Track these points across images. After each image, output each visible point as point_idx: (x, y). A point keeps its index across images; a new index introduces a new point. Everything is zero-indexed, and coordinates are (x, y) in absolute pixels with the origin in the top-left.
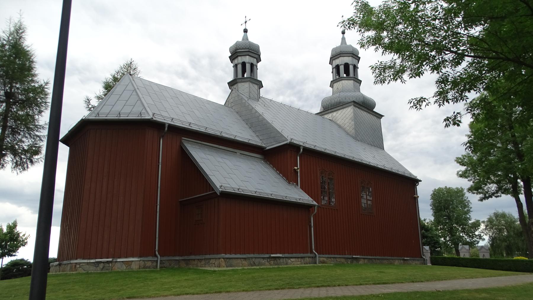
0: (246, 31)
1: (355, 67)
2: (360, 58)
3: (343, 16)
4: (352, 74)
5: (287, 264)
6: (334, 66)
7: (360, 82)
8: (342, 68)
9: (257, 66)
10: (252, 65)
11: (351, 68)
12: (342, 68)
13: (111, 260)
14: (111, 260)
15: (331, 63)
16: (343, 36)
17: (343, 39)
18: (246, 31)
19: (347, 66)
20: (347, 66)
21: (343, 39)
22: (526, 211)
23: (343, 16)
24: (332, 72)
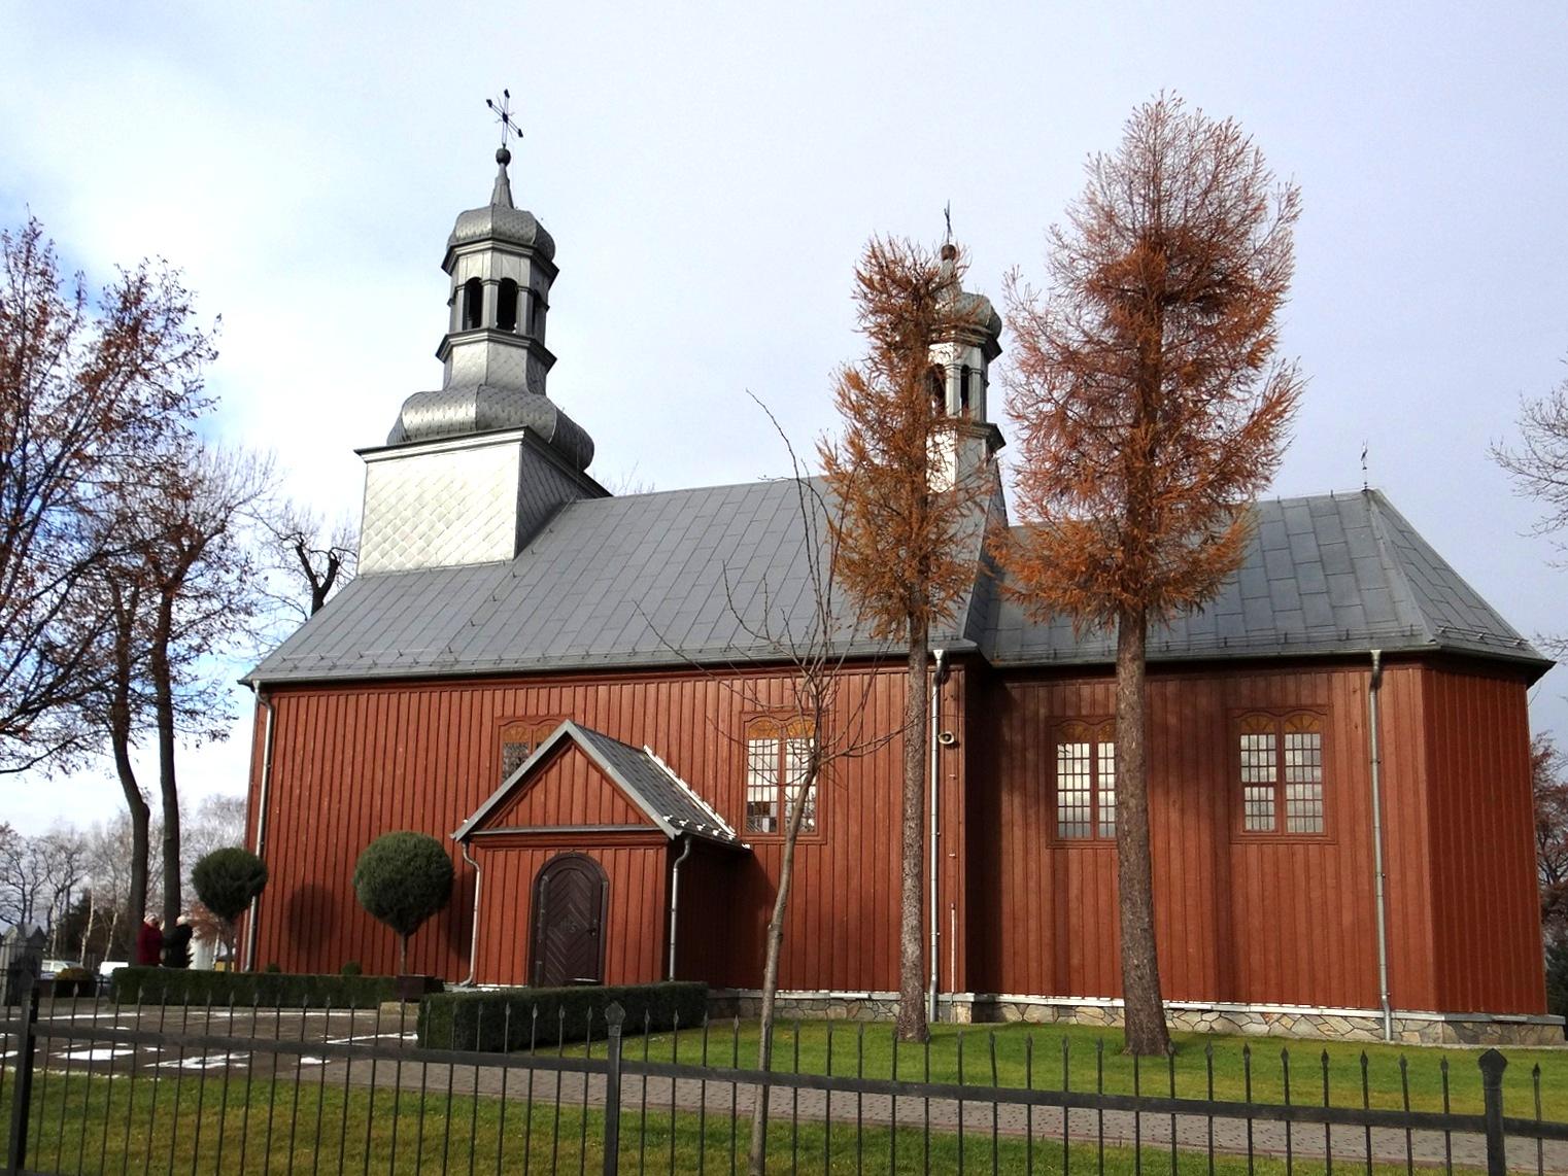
0: (504, 158)
1: (539, 305)
2: (557, 271)
3: (490, 103)
4: (521, 325)
5: (749, 1137)
6: (462, 281)
7: (548, 360)
8: (490, 295)
9: (984, 375)
10: (966, 372)
11: (523, 299)
12: (490, 295)
13: (864, 995)
14: (864, 995)
15: (450, 264)
16: (504, 174)
17: (504, 181)
18: (504, 158)
19: (507, 288)
20: (507, 288)
21: (504, 181)
22: (687, 983)
23: (490, 103)
24: (452, 302)
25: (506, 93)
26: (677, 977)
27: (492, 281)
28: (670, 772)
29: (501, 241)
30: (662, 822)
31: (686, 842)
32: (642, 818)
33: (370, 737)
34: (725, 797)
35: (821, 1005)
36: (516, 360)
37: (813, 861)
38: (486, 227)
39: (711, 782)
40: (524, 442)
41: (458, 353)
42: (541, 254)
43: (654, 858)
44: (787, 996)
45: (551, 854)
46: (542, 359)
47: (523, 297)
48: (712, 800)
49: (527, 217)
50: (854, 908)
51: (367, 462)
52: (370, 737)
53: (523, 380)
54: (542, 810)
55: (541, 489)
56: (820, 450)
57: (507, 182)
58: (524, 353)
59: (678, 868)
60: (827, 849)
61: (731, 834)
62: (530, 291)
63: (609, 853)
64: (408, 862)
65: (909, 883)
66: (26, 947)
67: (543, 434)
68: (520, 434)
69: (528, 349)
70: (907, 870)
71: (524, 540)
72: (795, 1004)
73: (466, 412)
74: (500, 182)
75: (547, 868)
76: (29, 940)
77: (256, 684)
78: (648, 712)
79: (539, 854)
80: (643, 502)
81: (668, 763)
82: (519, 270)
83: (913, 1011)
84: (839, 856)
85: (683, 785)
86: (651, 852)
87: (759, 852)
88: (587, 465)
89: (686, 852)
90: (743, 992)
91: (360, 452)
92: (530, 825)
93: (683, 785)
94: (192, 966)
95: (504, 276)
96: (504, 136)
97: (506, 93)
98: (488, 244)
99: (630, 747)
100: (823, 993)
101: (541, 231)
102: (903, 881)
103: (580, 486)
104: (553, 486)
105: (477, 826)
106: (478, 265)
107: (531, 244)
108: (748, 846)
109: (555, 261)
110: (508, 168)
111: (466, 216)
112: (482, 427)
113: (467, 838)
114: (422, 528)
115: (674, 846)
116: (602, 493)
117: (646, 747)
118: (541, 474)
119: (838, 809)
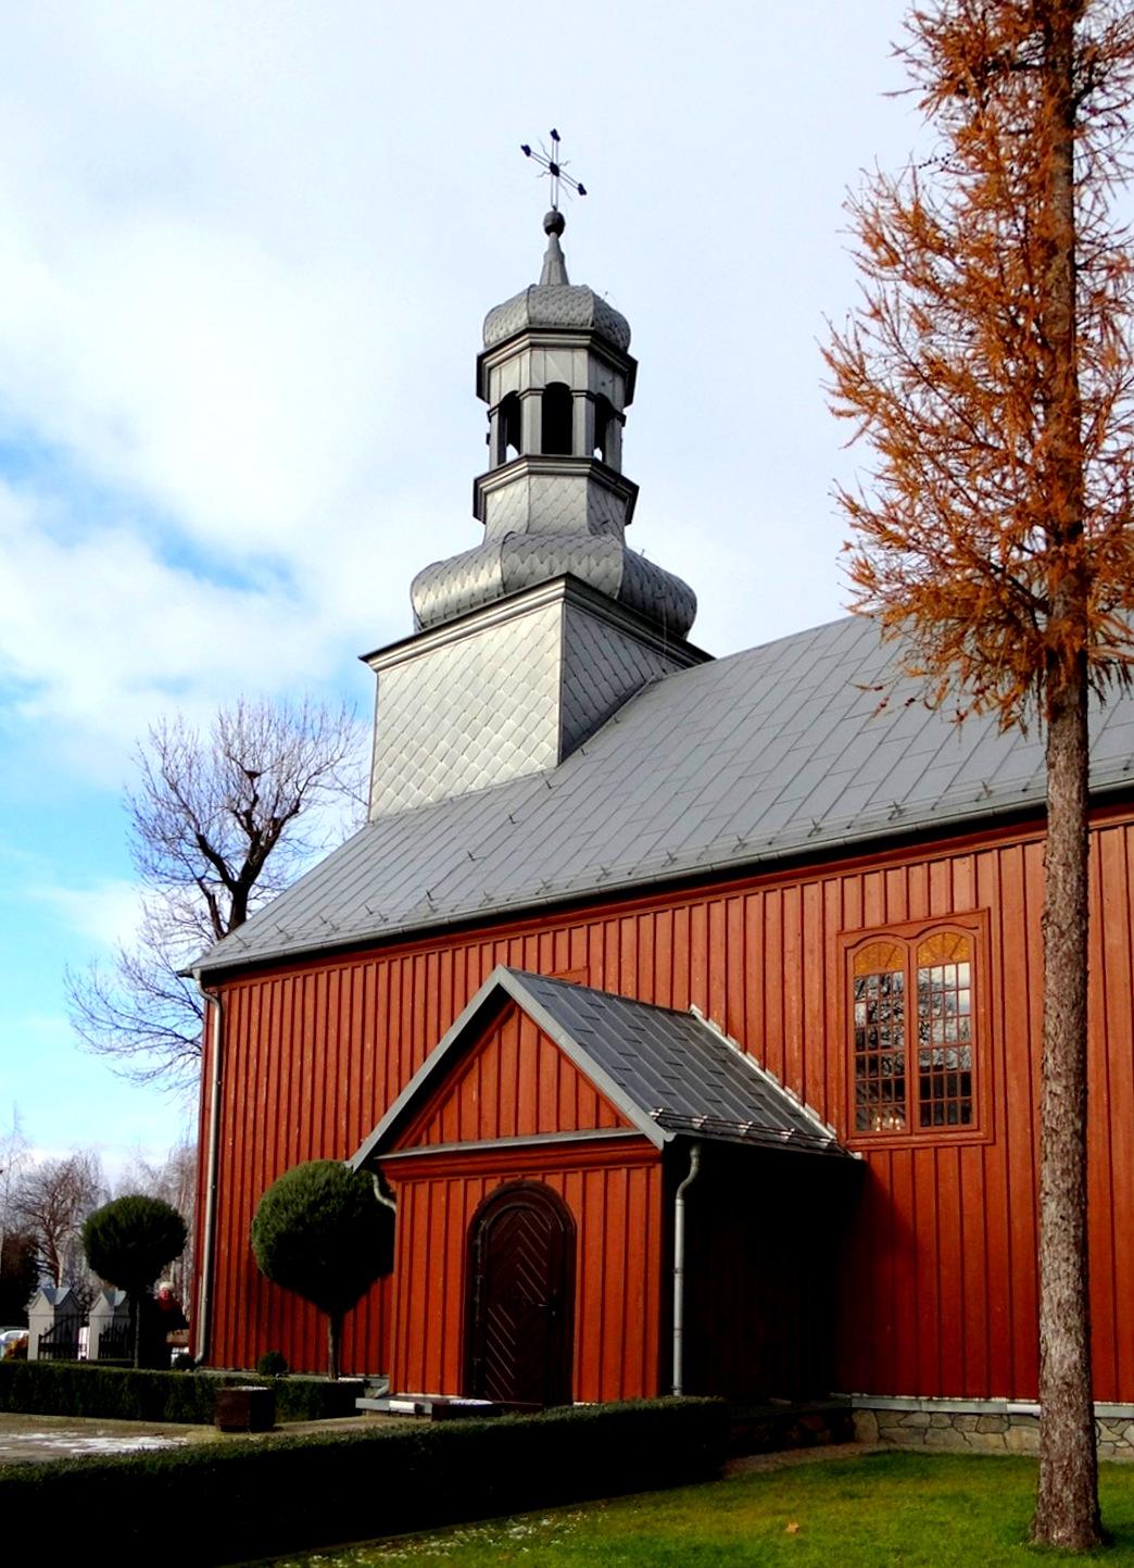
0: (556, 225)
7: (627, 493)
8: (532, 410)
12: (532, 410)
15: (482, 391)
18: (556, 225)
21: (558, 257)
25: (555, 135)
26: (685, 1390)
27: (532, 391)
28: (731, 1044)
29: (541, 334)
30: (644, 1122)
31: (694, 1153)
32: (619, 1120)
33: (333, 1032)
34: (819, 1076)
35: (995, 1424)
36: (570, 495)
37: (972, 1176)
38: (519, 320)
39: (797, 1054)
40: (567, 599)
41: (495, 502)
42: (607, 343)
43: (643, 1184)
44: (932, 1408)
45: (492, 1185)
46: (617, 492)
47: (581, 407)
48: (799, 1082)
49: (585, 292)
50: (974, 1265)
51: (377, 671)
52: (333, 1032)
53: (583, 518)
54: (482, 1120)
55: (604, 665)
56: (830, 359)
57: (561, 257)
58: (583, 482)
59: (685, 1197)
60: (996, 1153)
61: (829, 1133)
62: (589, 395)
63: (575, 1180)
64: (313, 1207)
65: (1051, 1210)
66: (115, 1317)
67: (605, 588)
68: (559, 588)
69: (589, 477)
70: (1047, 1185)
71: (570, 744)
72: (948, 1421)
73: (488, 577)
74: (551, 257)
75: (486, 1208)
76: (116, 1309)
77: (197, 973)
78: (694, 950)
79: (475, 1188)
80: (737, 659)
81: (728, 1030)
82: (573, 368)
83: (1066, 1481)
84: (1016, 1164)
85: (752, 1062)
86: (639, 1176)
87: (879, 1163)
88: (687, 628)
89: (693, 1169)
90: (859, 1400)
91: (366, 659)
92: (460, 1140)
93: (752, 1062)
94: (81, 1354)
95: (548, 382)
96: (554, 193)
97: (555, 135)
98: (525, 341)
99: (671, 1012)
100: (1000, 1403)
101: (600, 306)
102: (1036, 1213)
103: (668, 653)
104: (621, 656)
105: (385, 1143)
106: (511, 377)
107: (589, 327)
108: (858, 1155)
109: (631, 352)
110: (562, 239)
111: (494, 314)
112: (512, 590)
113: (370, 1163)
114: (444, 744)
115: (673, 1157)
116: (705, 657)
117: (693, 1007)
118: (604, 644)
119: (1012, 1082)
